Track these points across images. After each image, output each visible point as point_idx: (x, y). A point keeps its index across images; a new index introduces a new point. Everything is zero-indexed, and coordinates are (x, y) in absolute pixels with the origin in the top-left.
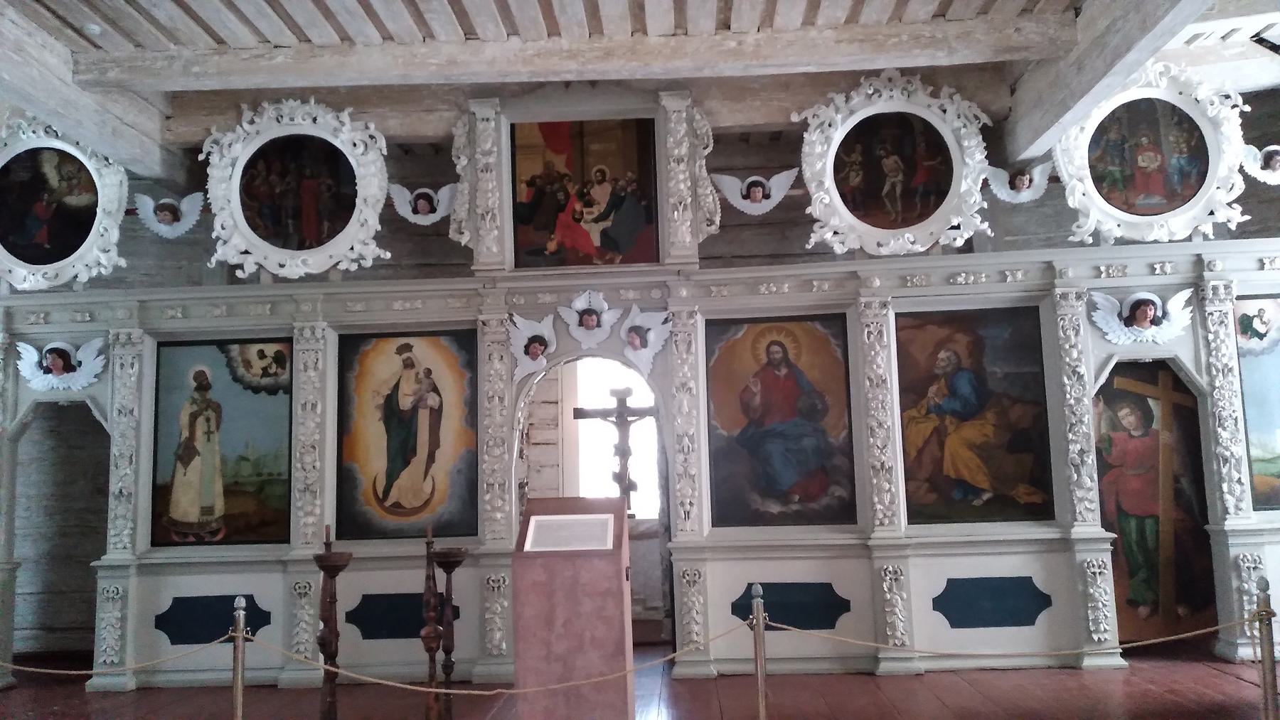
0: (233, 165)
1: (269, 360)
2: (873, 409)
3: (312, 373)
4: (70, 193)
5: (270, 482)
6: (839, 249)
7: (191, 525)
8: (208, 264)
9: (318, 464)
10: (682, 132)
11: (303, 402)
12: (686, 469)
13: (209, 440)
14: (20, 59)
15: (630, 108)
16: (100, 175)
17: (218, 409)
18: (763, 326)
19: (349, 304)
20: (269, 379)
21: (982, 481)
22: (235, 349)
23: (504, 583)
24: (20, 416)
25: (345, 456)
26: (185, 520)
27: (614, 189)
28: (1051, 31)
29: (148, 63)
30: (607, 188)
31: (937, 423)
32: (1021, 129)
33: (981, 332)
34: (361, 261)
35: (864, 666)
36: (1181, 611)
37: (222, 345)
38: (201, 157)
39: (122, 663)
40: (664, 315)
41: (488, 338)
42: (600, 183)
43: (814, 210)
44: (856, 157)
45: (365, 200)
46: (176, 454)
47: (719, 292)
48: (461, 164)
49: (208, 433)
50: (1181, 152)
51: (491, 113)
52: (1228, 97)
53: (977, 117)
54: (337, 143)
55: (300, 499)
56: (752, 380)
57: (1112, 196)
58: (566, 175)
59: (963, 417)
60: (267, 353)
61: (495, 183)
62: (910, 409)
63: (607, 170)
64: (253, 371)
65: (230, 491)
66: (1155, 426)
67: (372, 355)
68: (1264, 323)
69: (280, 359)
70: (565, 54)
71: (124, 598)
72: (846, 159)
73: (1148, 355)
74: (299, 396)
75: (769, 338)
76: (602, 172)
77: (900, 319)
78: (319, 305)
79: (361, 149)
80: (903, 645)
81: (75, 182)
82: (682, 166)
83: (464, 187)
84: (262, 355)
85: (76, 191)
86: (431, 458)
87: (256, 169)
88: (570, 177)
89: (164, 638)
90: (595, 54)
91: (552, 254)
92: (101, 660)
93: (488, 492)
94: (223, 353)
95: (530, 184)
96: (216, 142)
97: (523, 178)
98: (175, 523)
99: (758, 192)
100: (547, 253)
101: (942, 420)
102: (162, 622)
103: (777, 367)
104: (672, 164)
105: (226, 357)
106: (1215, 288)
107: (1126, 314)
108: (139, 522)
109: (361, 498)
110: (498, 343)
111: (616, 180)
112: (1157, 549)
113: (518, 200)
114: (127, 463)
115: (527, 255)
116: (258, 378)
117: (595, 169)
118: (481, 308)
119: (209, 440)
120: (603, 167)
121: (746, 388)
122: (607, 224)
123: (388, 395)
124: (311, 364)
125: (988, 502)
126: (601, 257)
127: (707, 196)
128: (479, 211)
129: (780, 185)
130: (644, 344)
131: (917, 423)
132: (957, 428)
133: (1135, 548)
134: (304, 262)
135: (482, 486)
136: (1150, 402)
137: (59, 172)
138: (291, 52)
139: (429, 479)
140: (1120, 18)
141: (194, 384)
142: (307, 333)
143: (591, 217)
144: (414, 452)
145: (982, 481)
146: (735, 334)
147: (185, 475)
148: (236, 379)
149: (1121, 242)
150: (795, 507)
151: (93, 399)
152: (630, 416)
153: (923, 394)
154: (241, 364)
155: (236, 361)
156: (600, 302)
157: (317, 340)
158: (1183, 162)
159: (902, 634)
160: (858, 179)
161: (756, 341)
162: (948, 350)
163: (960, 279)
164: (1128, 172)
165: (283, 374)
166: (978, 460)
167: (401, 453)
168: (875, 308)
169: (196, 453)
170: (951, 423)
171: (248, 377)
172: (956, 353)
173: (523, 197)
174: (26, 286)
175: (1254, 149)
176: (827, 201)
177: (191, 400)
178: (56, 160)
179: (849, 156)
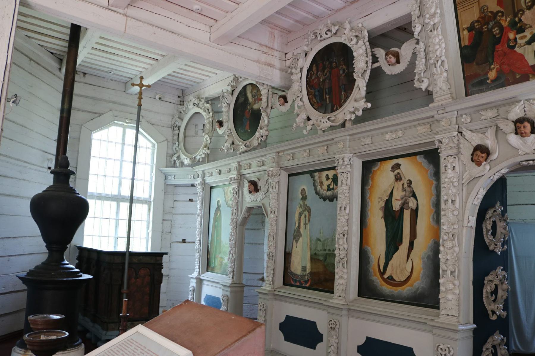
0: (301, 71)
19: (363, 140)
25: (364, 242)
37: (311, 173)
49: (305, 224)
58: (499, 12)
61: (440, 37)
64: (324, 187)
67: (378, 173)
78: (348, 143)
79: (355, 40)
81: (256, 97)
91: (493, 81)
97: (464, 26)
100: (488, 81)
109: (371, 270)
113: (463, 46)
123: (387, 200)
128: (432, 61)
133: (313, 19)
139: (410, 260)
141: (301, 196)
142: (341, 162)
143: (524, 41)
144: (401, 242)
148: (317, 193)
173: (466, 43)
177: (299, 206)
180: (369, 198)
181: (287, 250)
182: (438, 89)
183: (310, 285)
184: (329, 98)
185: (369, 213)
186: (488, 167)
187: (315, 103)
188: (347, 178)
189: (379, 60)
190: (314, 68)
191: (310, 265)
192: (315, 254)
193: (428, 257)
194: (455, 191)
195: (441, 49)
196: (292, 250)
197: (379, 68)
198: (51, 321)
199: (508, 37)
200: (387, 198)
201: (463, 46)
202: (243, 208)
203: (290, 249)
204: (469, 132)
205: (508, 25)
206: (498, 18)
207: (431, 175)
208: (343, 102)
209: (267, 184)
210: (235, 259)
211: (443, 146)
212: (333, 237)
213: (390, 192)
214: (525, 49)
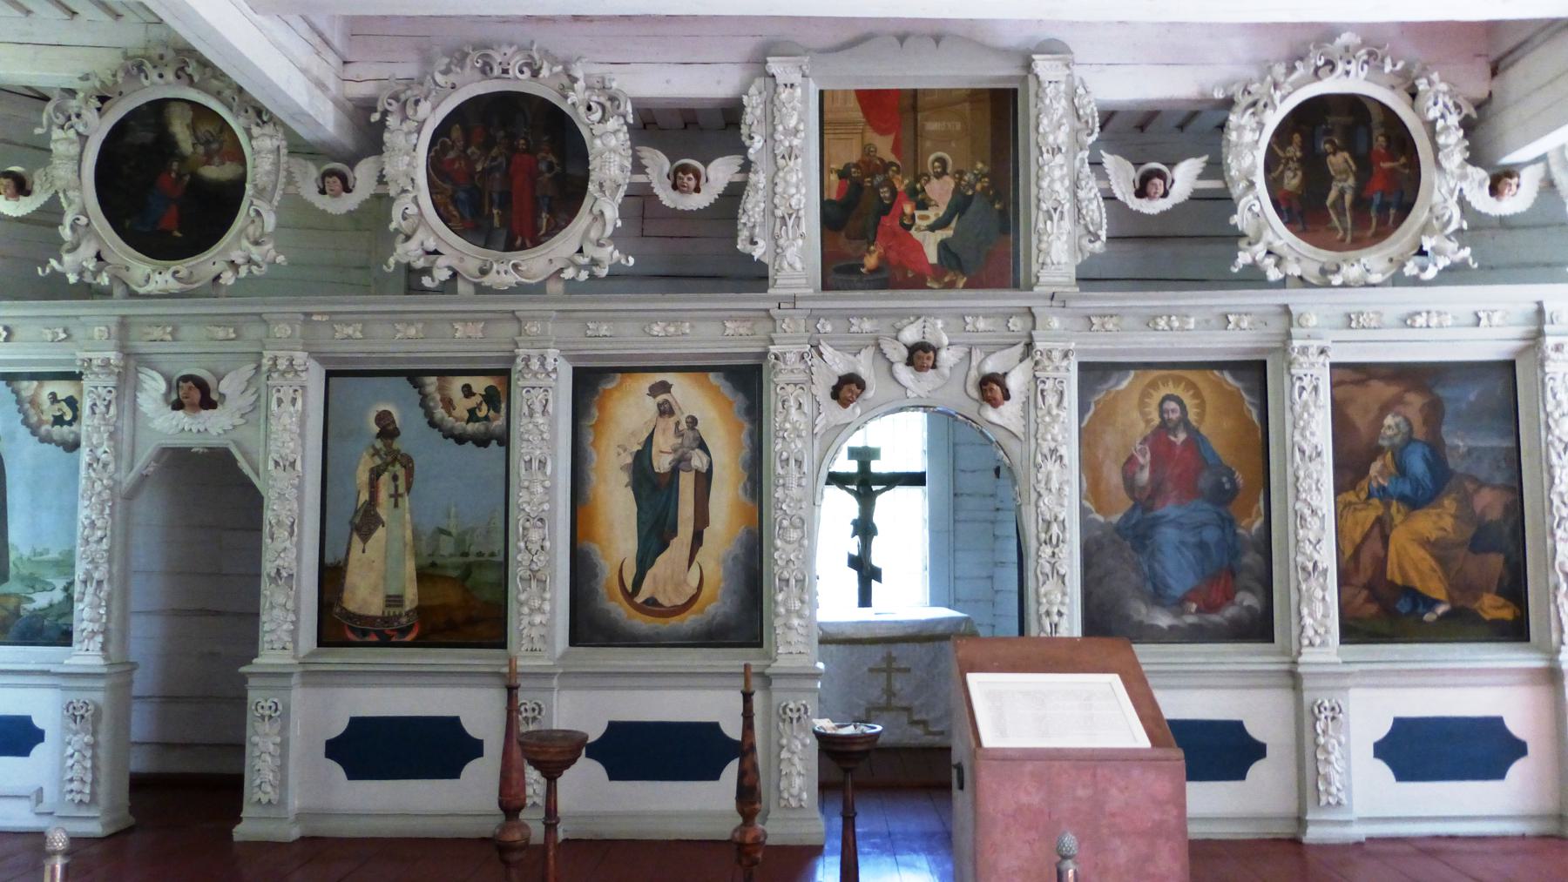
0: (419, 132)
1: (477, 399)
2: (1305, 491)
3: (540, 420)
4: (208, 162)
5: (480, 565)
6: (1273, 274)
8: (385, 267)
9: (547, 544)
10: (1060, 111)
11: (527, 458)
12: (1053, 566)
13: (396, 505)
15: (989, 72)
16: (251, 137)
17: (408, 464)
18: (1156, 373)
19: (591, 325)
20: (477, 424)
22: (431, 383)
23: (806, 712)
24: (135, 469)
27: (958, 185)
30: (949, 183)
31: (1380, 512)
32: (1509, 121)
33: (1440, 392)
34: (594, 269)
35: (1283, 830)
37: (414, 377)
38: (375, 117)
39: (282, 803)
41: (781, 379)
42: (938, 176)
43: (1241, 220)
44: (1294, 151)
45: (601, 185)
46: (351, 522)
47: (1103, 325)
49: (396, 496)
51: (796, 78)
55: (524, 590)
56: (1138, 447)
58: (892, 164)
59: (1414, 503)
60: (474, 389)
61: (800, 175)
62: (1347, 491)
63: (950, 162)
64: (456, 413)
65: (426, 575)
67: (616, 395)
69: (491, 398)
71: (285, 716)
74: (521, 450)
75: (1164, 392)
76: (942, 161)
77: (1338, 372)
80: (1339, 803)
81: (215, 146)
82: (1059, 159)
84: (468, 391)
85: (216, 159)
87: (449, 137)
88: (898, 166)
89: (338, 771)
91: (872, 272)
92: (255, 798)
93: (781, 590)
94: (415, 387)
95: (843, 174)
97: (832, 166)
98: (351, 616)
100: (863, 270)
102: (335, 749)
103: (1174, 431)
104: (1045, 155)
105: (420, 393)
108: (303, 618)
109: (602, 590)
110: (796, 385)
111: (961, 173)
113: (826, 198)
114: (286, 534)
116: (463, 424)
117: (932, 157)
118: (773, 335)
119: (396, 505)
120: (940, 154)
121: (1131, 460)
124: (538, 407)
125: (1445, 616)
126: (938, 279)
127: (1090, 200)
131: (1355, 509)
132: (1407, 516)
134: (515, 266)
139: (695, 568)
141: (377, 429)
142: (535, 364)
143: (924, 223)
144: (674, 532)
145: (1435, 588)
146: (1118, 383)
147: (364, 551)
148: (433, 424)
150: (1191, 619)
151: (238, 444)
152: (875, 485)
154: (441, 405)
155: (433, 399)
156: (938, 332)
157: (548, 374)
159: (1338, 790)
160: (1295, 182)
161: (1145, 395)
162: (1397, 414)
163: (1420, 321)
165: (495, 420)
166: (1433, 563)
168: (1313, 354)
170: (1398, 511)
174: (151, 288)
176: (1256, 209)
177: (371, 451)
178: (189, 114)
179: (1283, 148)
180: (593, 444)
181: (329, 559)
183: (418, 637)
184: (501, 217)
185: (594, 477)
186: (858, 411)
187: (454, 216)
188: (547, 401)
189: (647, 170)
191: (415, 590)
192: (433, 565)
193: (735, 558)
194: (800, 446)
195: (798, 196)
197: (647, 186)
198: (560, 735)
199: (902, 209)
200: (640, 448)
201: (826, 198)
202: (138, 450)
203: (342, 556)
204: (830, 349)
205: (905, 191)
206: (891, 173)
207: (739, 412)
208: (544, 235)
209: (252, 390)
210: (110, 595)
211: (781, 365)
212: (489, 524)
214: (925, 236)
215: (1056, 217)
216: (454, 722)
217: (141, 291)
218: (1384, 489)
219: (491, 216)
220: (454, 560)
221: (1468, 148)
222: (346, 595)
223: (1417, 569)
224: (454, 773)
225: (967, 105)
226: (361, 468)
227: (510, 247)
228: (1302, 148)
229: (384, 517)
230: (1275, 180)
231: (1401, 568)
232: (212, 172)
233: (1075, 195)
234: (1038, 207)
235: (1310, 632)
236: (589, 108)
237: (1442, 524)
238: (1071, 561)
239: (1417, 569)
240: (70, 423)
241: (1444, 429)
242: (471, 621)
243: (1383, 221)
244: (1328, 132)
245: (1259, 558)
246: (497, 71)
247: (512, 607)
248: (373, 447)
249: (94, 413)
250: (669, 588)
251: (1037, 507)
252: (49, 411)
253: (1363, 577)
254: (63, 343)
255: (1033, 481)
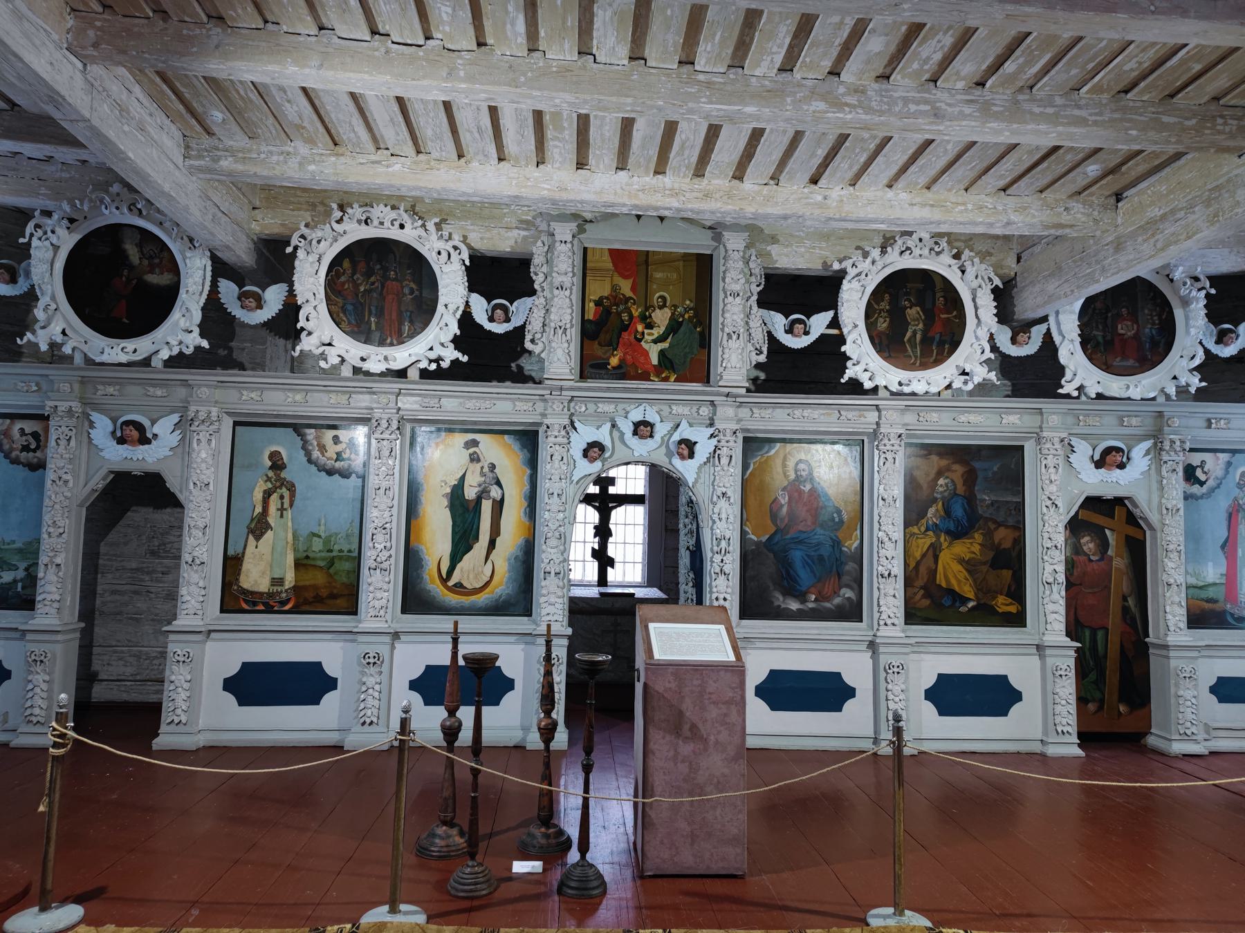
0: (319, 260)
4: (152, 272)
5: (341, 558)
7: (262, 594)
13: (282, 516)
14: (143, 139)
15: (700, 243)
17: (292, 488)
21: (968, 591)
26: (256, 589)
27: (673, 314)
28: (1096, 213)
29: (263, 156)
30: (667, 313)
31: (934, 540)
36: (1122, 708)
37: (298, 429)
40: (711, 430)
42: (661, 308)
44: (885, 305)
48: (538, 280)
49: (282, 510)
50: (1153, 324)
52: (1197, 279)
53: (990, 280)
54: (424, 251)
57: (1094, 356)
58: (631, 298)
59: (957, 534)
62: (912, 526)
63: (668, 298)
66: (1110, 553)
68: (1205, 473)
70: (667, 192)
72: (876, 307)
73: (1108, 493)
82: (738, 300)
83: (538, 300)
85: (157, 270)
86: (492, 544)
89: (231, 699)
90: (695, 194)
91: (614, 368)
95: (598, 303)
96: (303, 237)
98: (245, 592)
99: (799, 328)
101: (938, 537)
102: (230, 685)
106: (1172, 442)
107: (1097, 457)
109: (426, 577)
111: (676, 307)
112: (1105, 656)
115: (591, 367)
117: (657, 295)
119: (282, 516)
122: (665, 345)
125: (973, 608)
126: (658, 374)
129: (819, 324)
130: (691, 455)
132: (950, 544)
135: (538, 575)
136: (1107, 532)
137: (141, 251)
138: (408, 162)
139: (489, 562)
140: (1181, 209)
141: (270, 464)
143: (651, 338)
144: (477, 539)
145: (968, 591)
148: (310, 461)
149: (1100, 396)
150: (811, 605)
153: (923, 514)
155: (312, 444)
158: (1154, 332)
160: (885, 325)
162: (947, 478)
164: (1109, 338)
167: (463, 540)
169: (268, 527)
170: (945, 540)
171: (323, 460)
172: (953, 481)
173: (590, 315)
175: (1212, 326)
177: (265, 478)
179: (878, 304)
182: (556, 359)
184: (377, 323)
190: (346, 264)
192: (307, 557)
196: (244, 553)
213: (461, 474)
215: (735, 337)
216: (318, 665)
217: (98, 360)
218: (936, 525)
219: (369, 323)
220: (323, 554)
221: (995, 307)
222: (242, 578)
223: (955, 577)
224: (316, 701)
225: (681, 263)
226: (257, 489)
227: (382, 343)
228: (890, 304)
229: (273, 525)
230: (872, 323)
231: (946, 577)
232: (153, 279)
233: (747, 323)
234: (723, 330)
235: (884, 616)
236: (439, 253)
237: (973, 549)
238: (732, 564)
239: (955, 577)
240: (34, 451)
241: (976, 488)
242: (333, 596)
243: (940, 353)
244: (907, 294)
245: (855, 566)
246: (376, 222)
247: (363, 587)
248: (267, 475)
249: (58, 444)
250: (471, 576)
251: (712, 529)
252: (19, 441)
253: (920, 583)
254: (35, 394)
255: (711, 513)
